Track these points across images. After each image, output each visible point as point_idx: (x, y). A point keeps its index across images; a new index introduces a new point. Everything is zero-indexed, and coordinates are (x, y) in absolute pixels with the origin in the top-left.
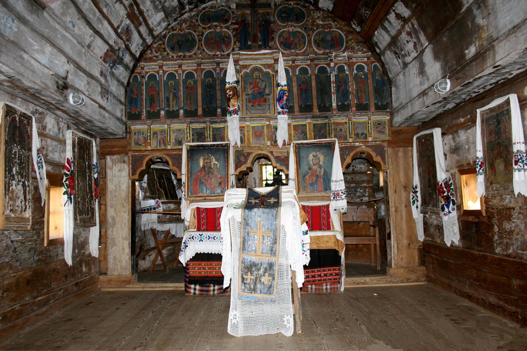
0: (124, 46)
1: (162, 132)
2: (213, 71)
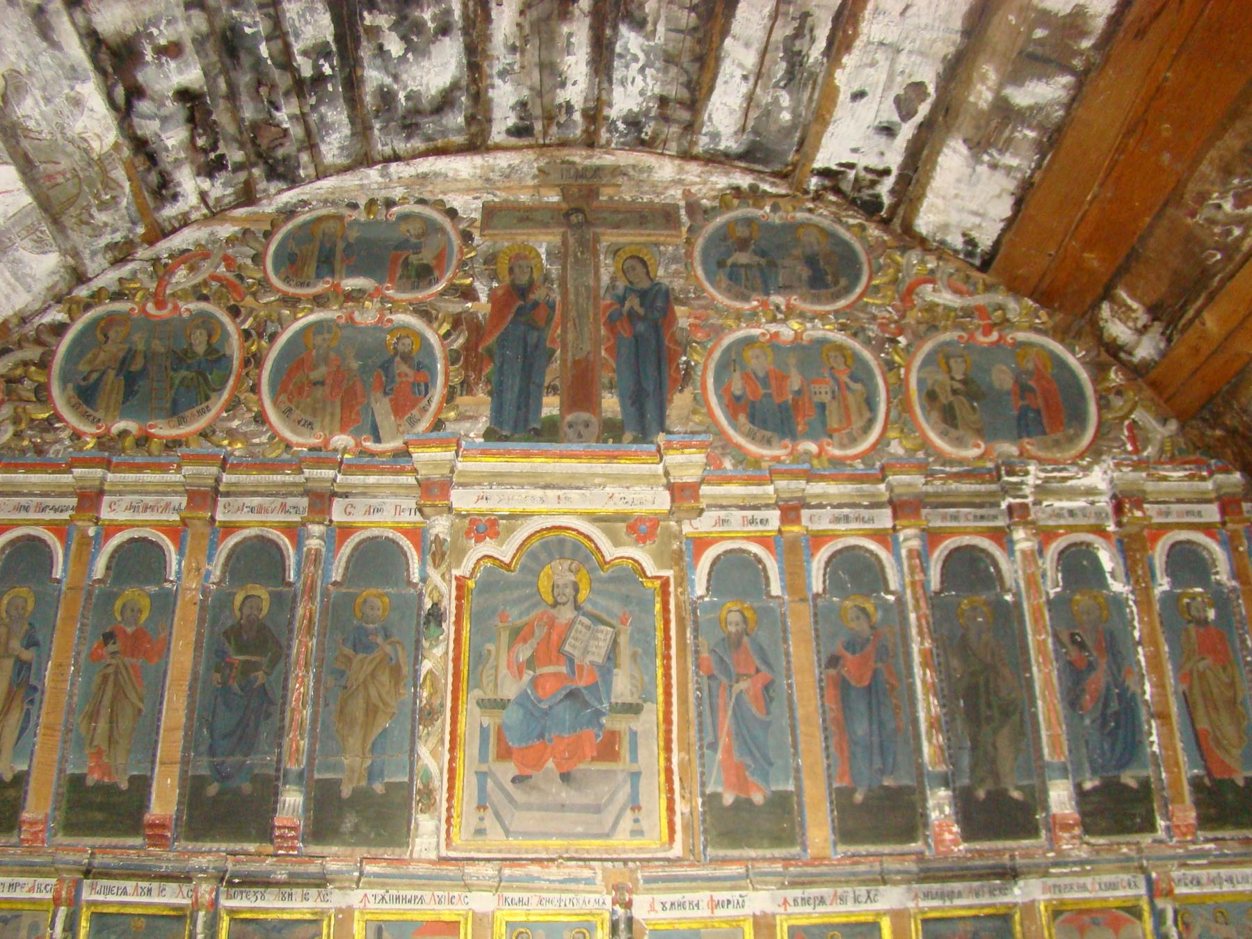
2: (285, 542)
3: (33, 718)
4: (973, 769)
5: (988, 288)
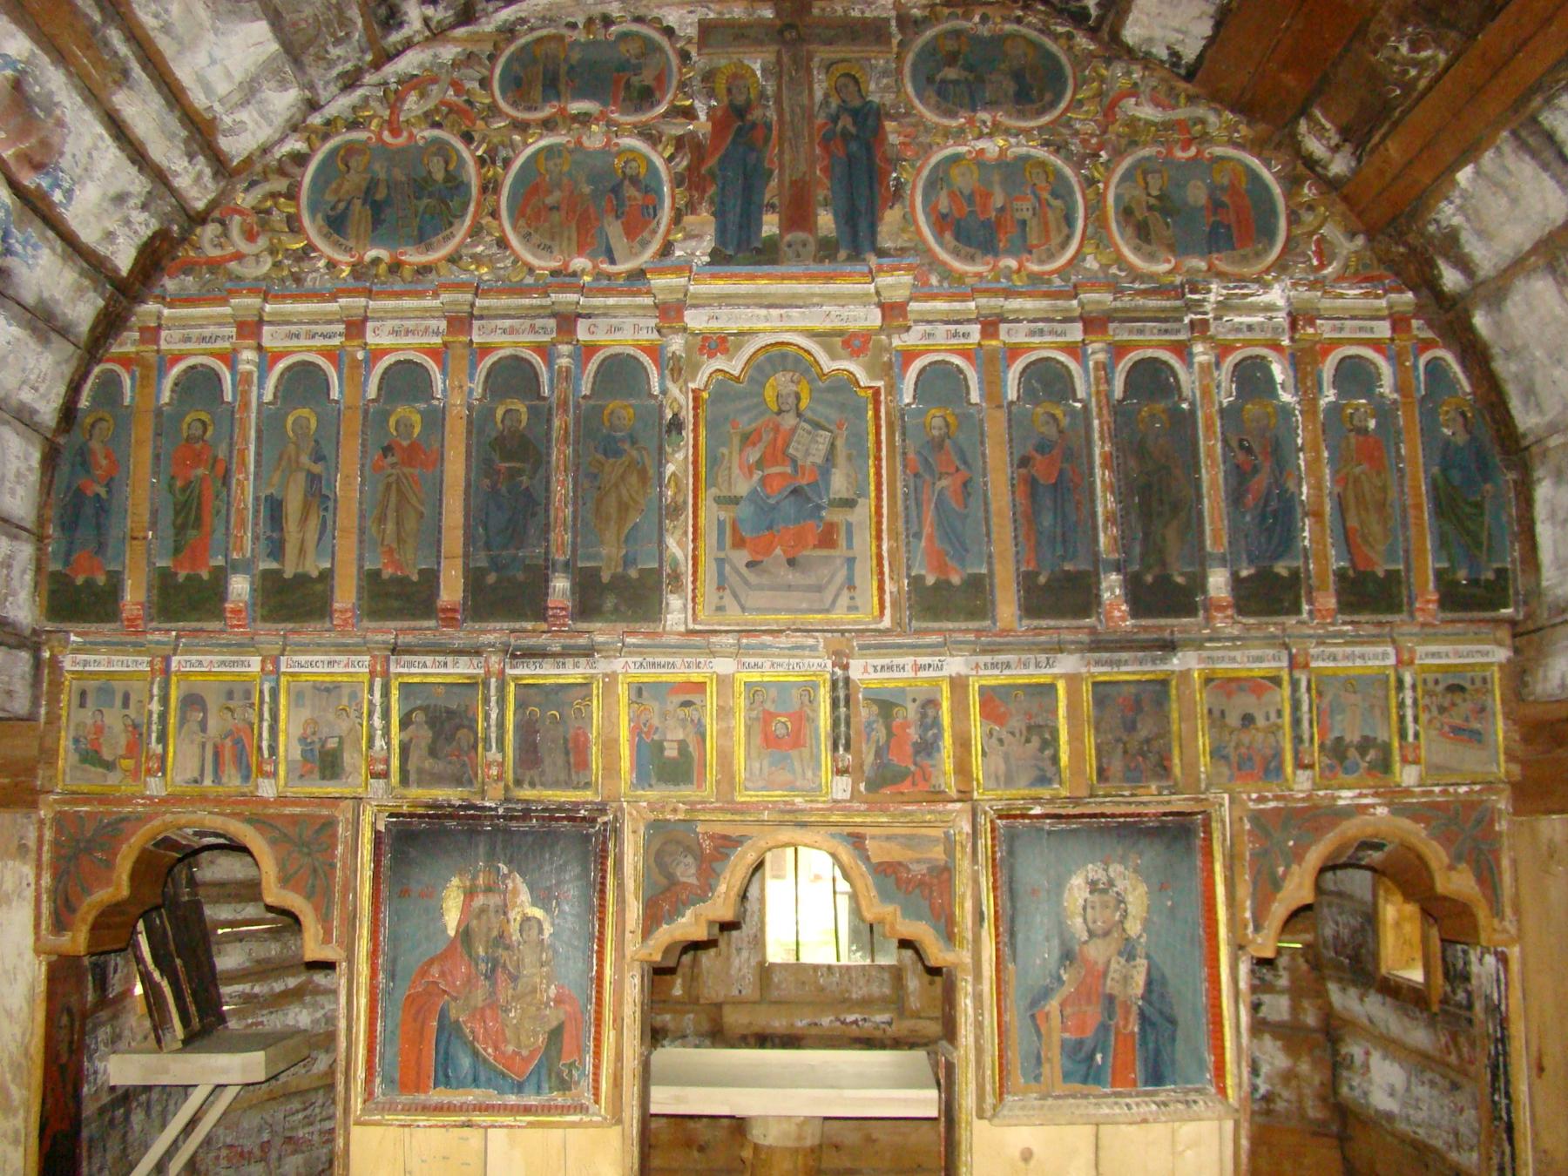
1: (230, 695)
2: (537, 360)
3: (330, 523)
5: (1192, 100)
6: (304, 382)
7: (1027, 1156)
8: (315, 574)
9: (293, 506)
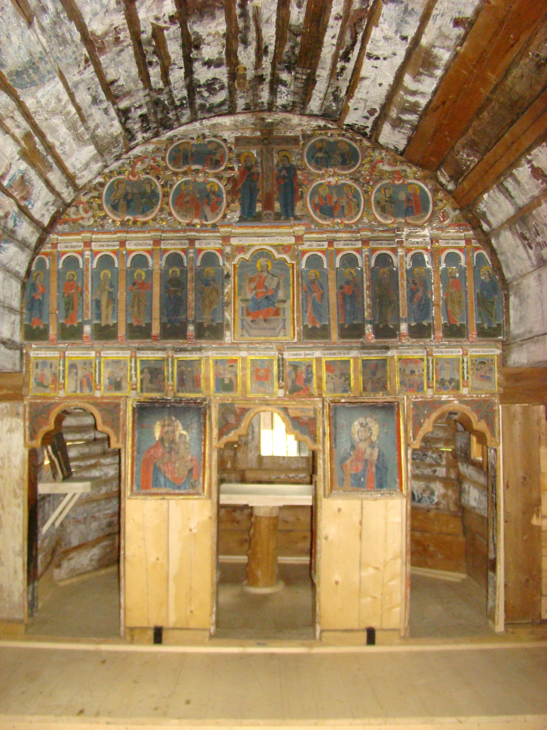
0: (16, 209)
1: (85, 364)
2: (182, 254)
4: (379, 318)
5: (402, 163)
6: (106, 261)
7: (339, 510)
8: (111, 324)
9: (104, 303)
